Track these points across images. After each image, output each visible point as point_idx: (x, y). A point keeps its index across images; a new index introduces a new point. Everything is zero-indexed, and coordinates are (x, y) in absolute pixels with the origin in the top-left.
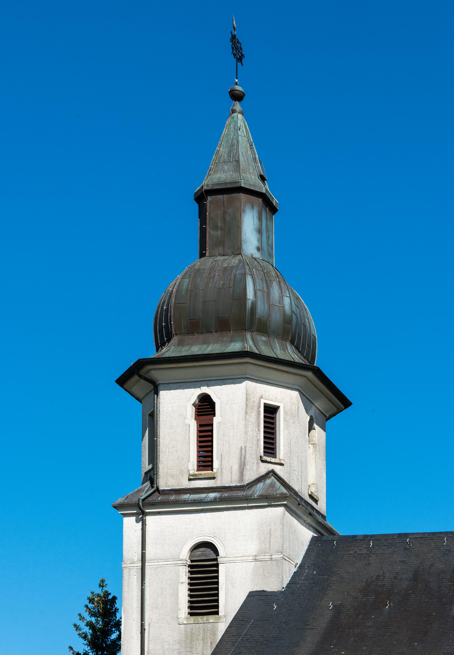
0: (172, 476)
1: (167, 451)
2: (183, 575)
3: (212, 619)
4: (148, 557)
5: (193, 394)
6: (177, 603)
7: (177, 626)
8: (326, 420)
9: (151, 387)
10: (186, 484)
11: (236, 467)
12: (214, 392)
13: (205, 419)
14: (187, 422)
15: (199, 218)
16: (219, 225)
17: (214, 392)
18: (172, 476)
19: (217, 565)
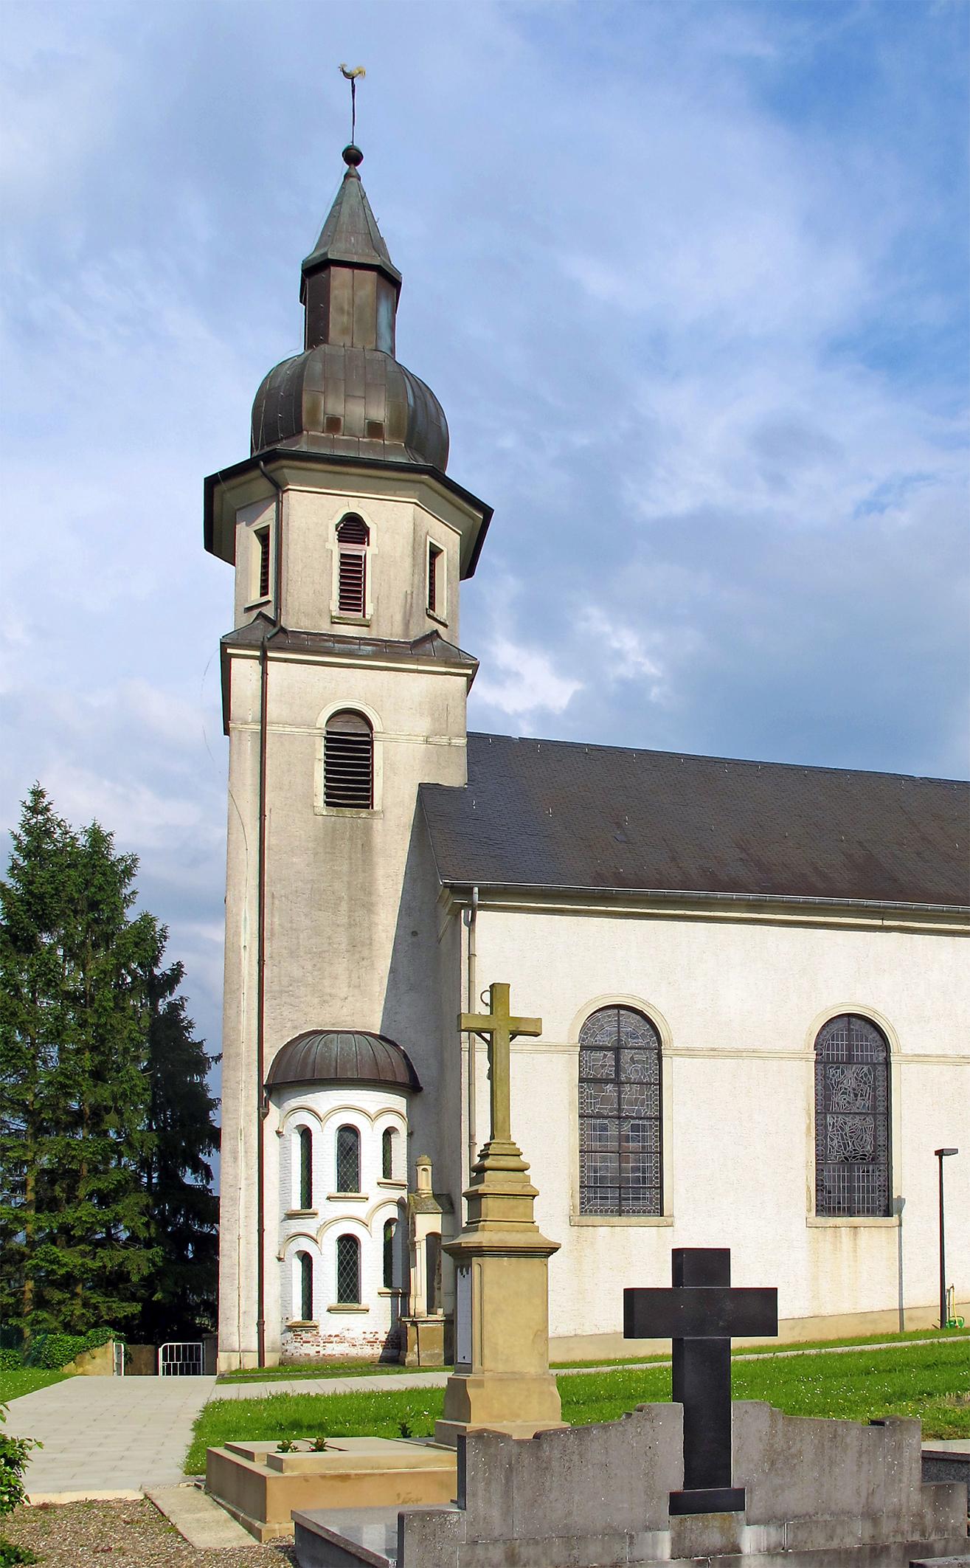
0: (306, 615)
1: (74, 978)
2: (320, 745)
3: (364, 813)
4: (271, 715)
5: (337, 506)
6: (312, 787)
7: (311, 816)
8: (511, 1039)
9: (273, 488)
10: (325, 627)
11: (398, 617)
12: (370, 509)
13: (352, 549)
14: (328, 546)
15: (303, 300)
16: (346, 308)
17: (370, 509)
18: (306, 615)
19: (371, 743)
